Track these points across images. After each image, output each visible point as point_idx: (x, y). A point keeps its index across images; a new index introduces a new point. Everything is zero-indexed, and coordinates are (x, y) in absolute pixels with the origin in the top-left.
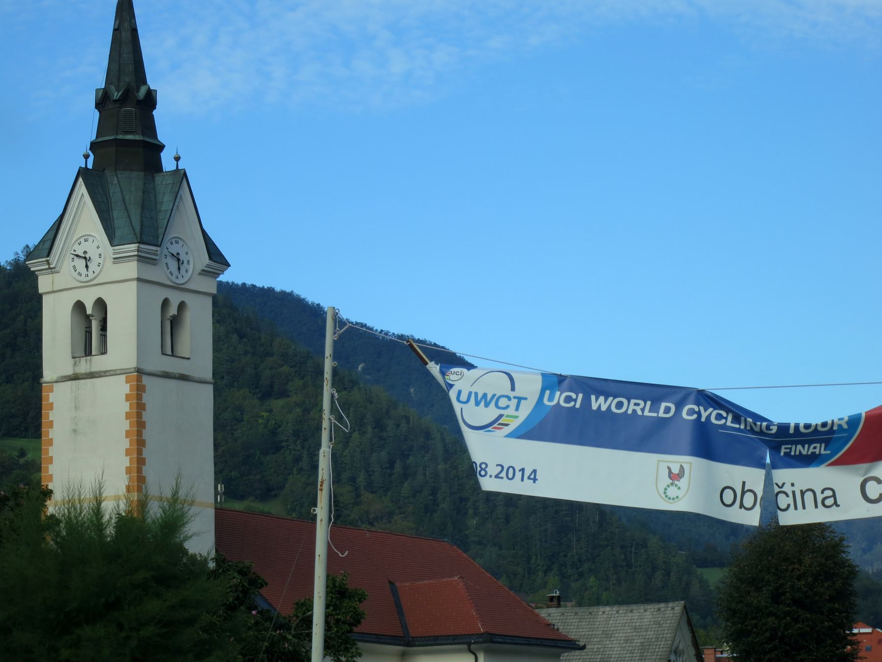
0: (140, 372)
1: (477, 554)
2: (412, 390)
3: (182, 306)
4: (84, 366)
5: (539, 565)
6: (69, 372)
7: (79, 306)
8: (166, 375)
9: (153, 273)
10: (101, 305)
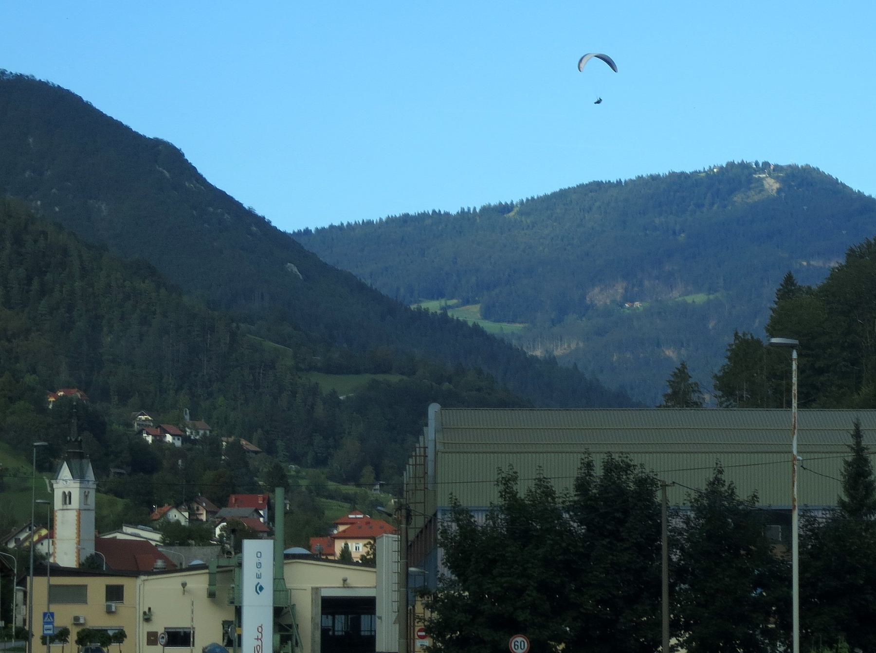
0: (79, 510)
1: (111, 372)
2: (31, 140)
3: (89, 492)
4: (65, 507)
5: (171, 384)
6: (61, 508)
7: (64, 493)
8: (85, 510)
9: (83, 486)
10: (70, 493)
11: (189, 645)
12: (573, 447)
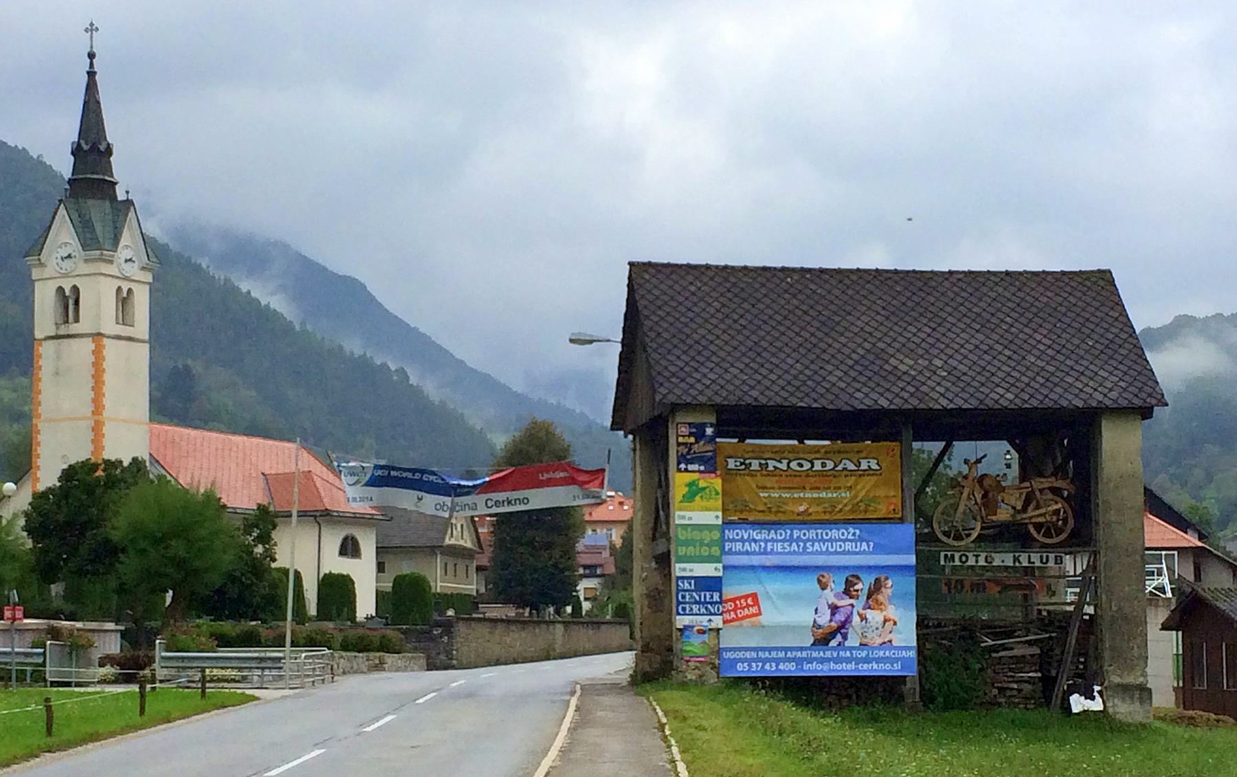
3: (130, 291)
7: (60, 290)
8: (119, 338)
10: (75, 289)
11: (150, 421)
12: (490, 546)
